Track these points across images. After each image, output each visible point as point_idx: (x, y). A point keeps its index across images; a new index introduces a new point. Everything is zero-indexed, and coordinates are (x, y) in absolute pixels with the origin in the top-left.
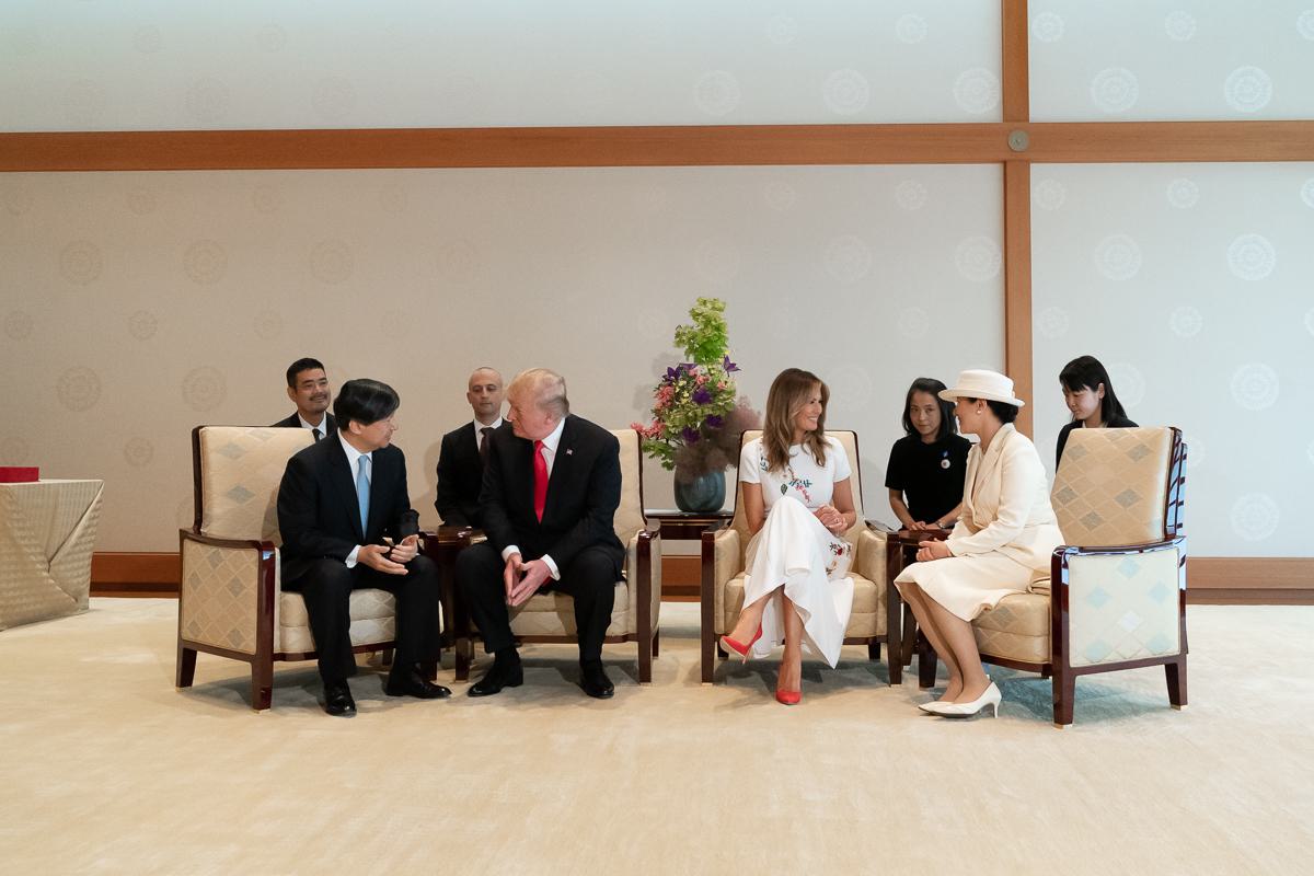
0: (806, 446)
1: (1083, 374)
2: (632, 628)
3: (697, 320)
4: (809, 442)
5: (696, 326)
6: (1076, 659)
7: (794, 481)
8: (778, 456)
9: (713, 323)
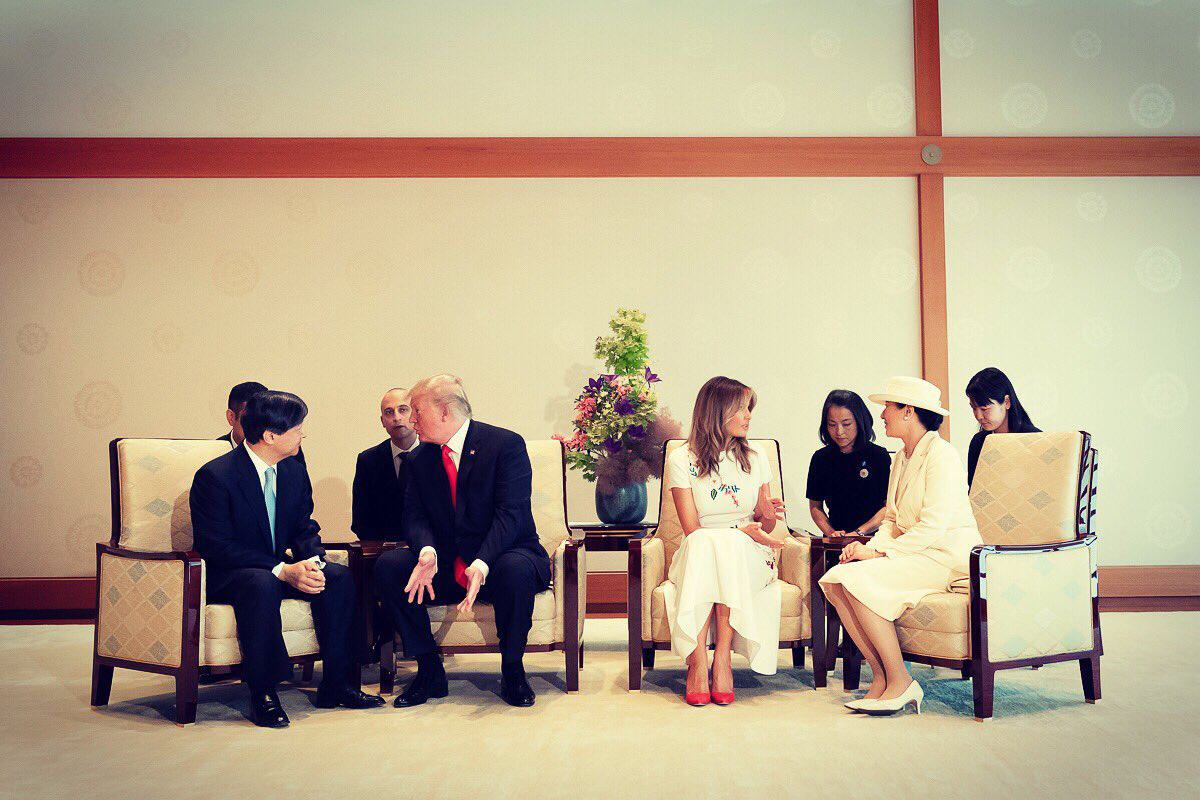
0: (730, 453)
1: (988, 387)
2: (559, 636)
3: (617, 331)
4: (734, 450)
5: (616, 338)
6: (995, 654)
8: (707, 463)
9: (634, 334)
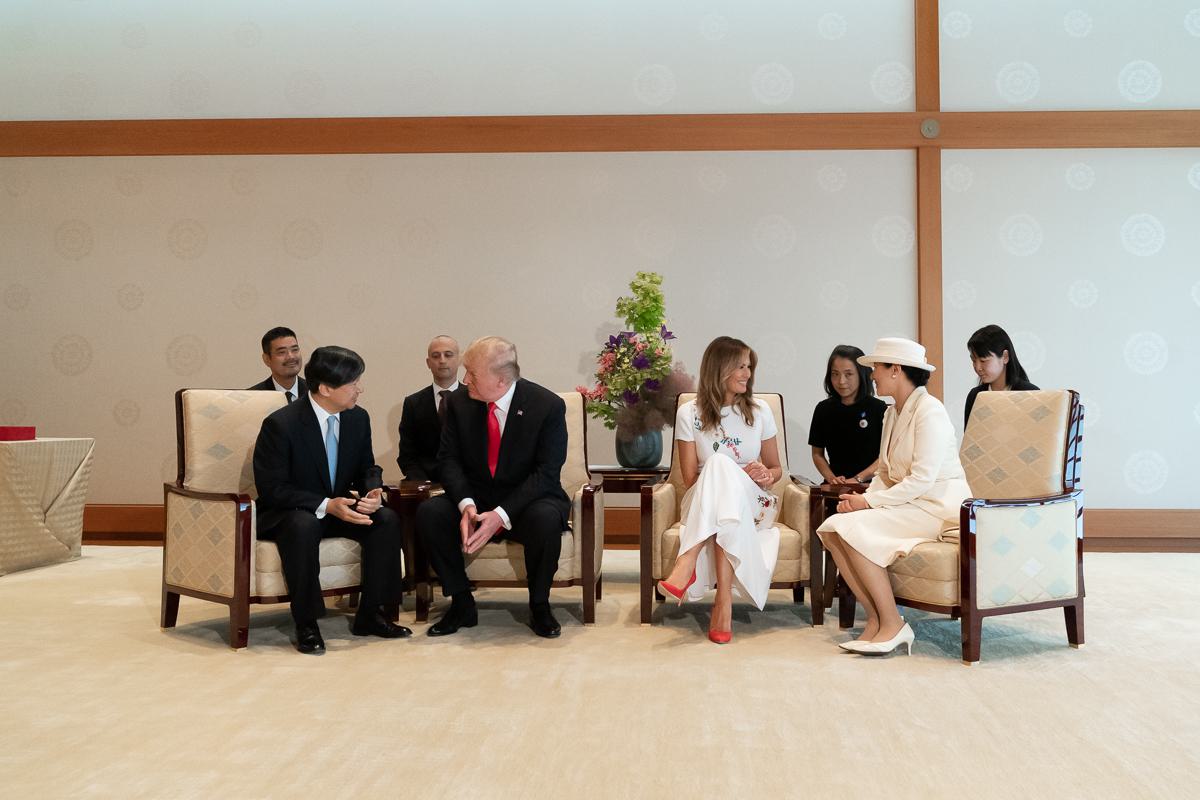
0: (736, 408)
1: (989, 342)
2: (577, 574)
3: (637, 292)
4: (739, 404)
5: (636, 298)
6: (983, 601)
7: (726, 439)
8: (710, 417)
9: (651, 295)
